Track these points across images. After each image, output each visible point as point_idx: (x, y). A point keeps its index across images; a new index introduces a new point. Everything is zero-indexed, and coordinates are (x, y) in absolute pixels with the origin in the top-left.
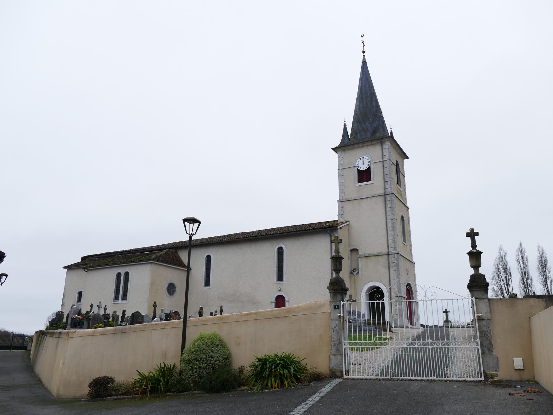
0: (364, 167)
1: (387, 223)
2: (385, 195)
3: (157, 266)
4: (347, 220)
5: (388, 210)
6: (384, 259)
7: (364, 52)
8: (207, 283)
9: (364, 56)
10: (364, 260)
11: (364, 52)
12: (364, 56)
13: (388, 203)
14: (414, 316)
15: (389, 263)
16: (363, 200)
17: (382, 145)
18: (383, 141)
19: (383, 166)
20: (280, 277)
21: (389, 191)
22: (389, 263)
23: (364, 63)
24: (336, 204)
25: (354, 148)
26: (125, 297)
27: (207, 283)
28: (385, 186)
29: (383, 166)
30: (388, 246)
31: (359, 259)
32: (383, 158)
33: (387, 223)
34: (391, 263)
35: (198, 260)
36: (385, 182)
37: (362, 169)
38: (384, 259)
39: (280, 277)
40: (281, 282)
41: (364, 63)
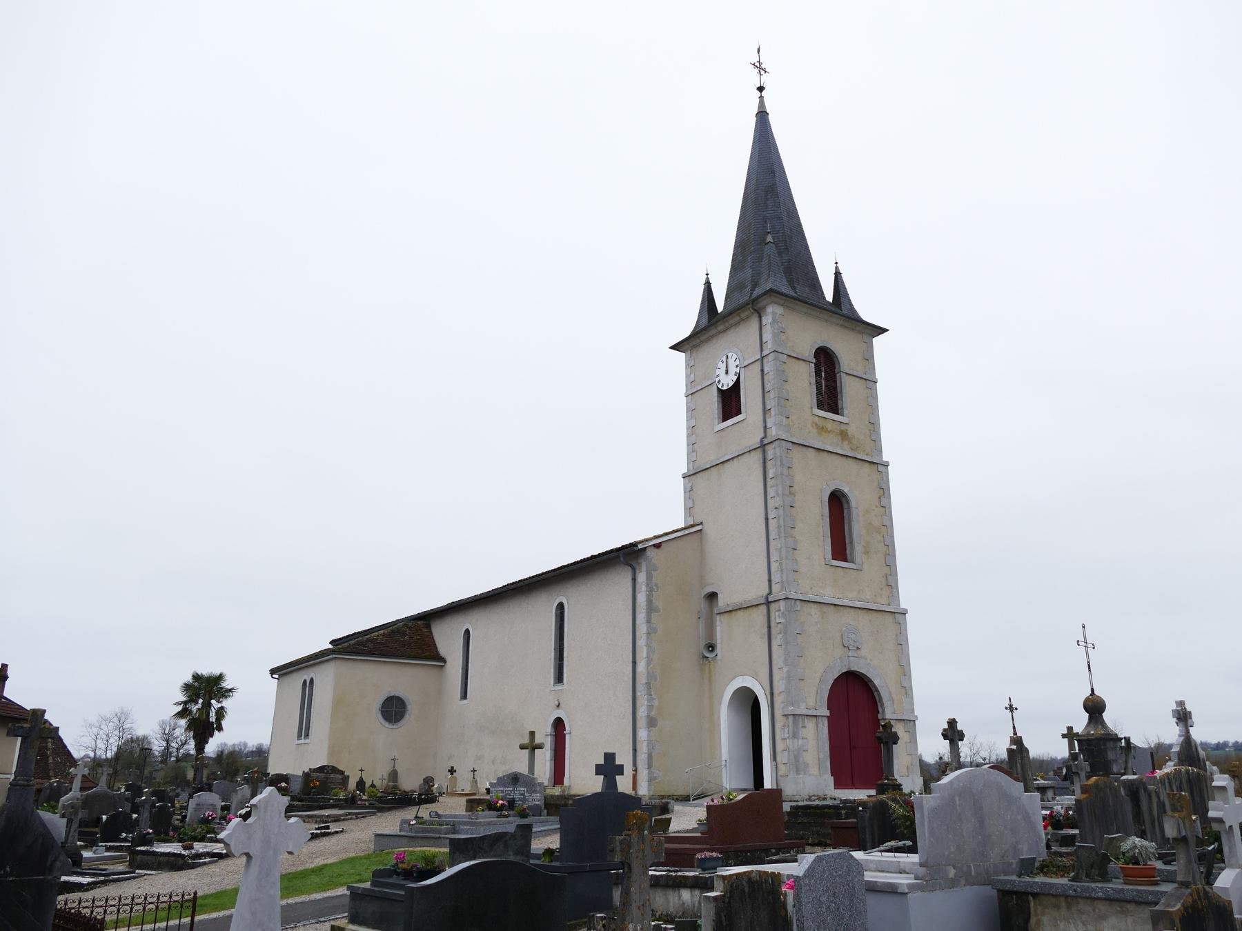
0: (727, 382)
1: (767, 519)
2: (763, 446)
3: (350, 664)
4: (698, 520)
5: (770, 483)
6: (759, 615)
7: (761, 89)
8: (464, 696)
9: (761, 97)
10: (725, 618)
11: (761, 89)
12: (761, 97)
13: (769, 464)
14: (419, 841)
15: (769, 627)
16: (726, 465)
17: (760, 317)
18: (760, 305)
19: (762, 371)
20: (559, 678)
21: (773, 433)
22: (769, 627)
23: (762, 115)
24: (679, 485)
25: (712, 337)
26: (307, 735)
27: (464, 696)
28: (765, 421)
29: (762, 371)
30: (770, 581)
31: (718, 617)
32: (762, 350)
33: (767, 519)
34: (773, 624)
35: (447, 638)
36: (765, 411)
37: (725, 388)
38: (759, 615)
39: (559, 678)
40: (559, 687)
41: (762, 115)
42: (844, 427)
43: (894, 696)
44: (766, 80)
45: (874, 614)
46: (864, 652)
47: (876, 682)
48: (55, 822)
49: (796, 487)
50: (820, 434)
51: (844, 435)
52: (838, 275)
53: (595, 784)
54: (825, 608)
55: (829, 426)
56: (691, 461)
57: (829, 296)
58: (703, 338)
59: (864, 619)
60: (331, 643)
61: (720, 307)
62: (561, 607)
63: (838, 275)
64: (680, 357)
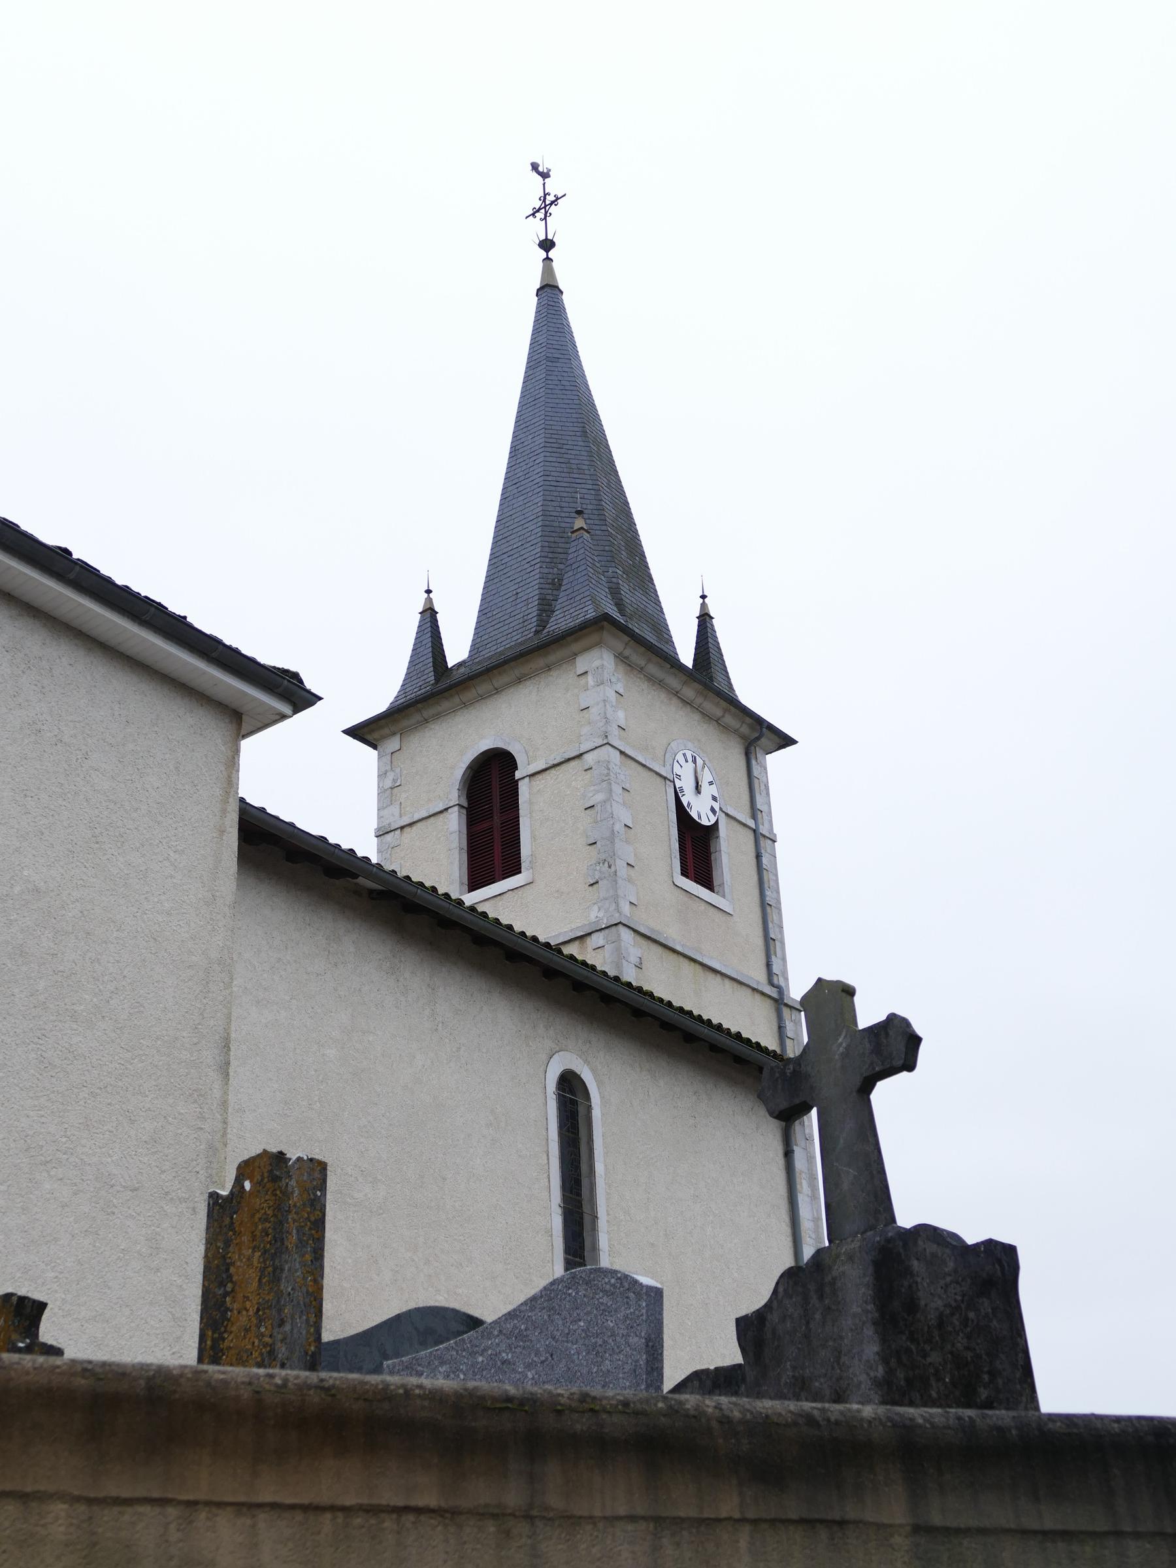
11: (547, 245)
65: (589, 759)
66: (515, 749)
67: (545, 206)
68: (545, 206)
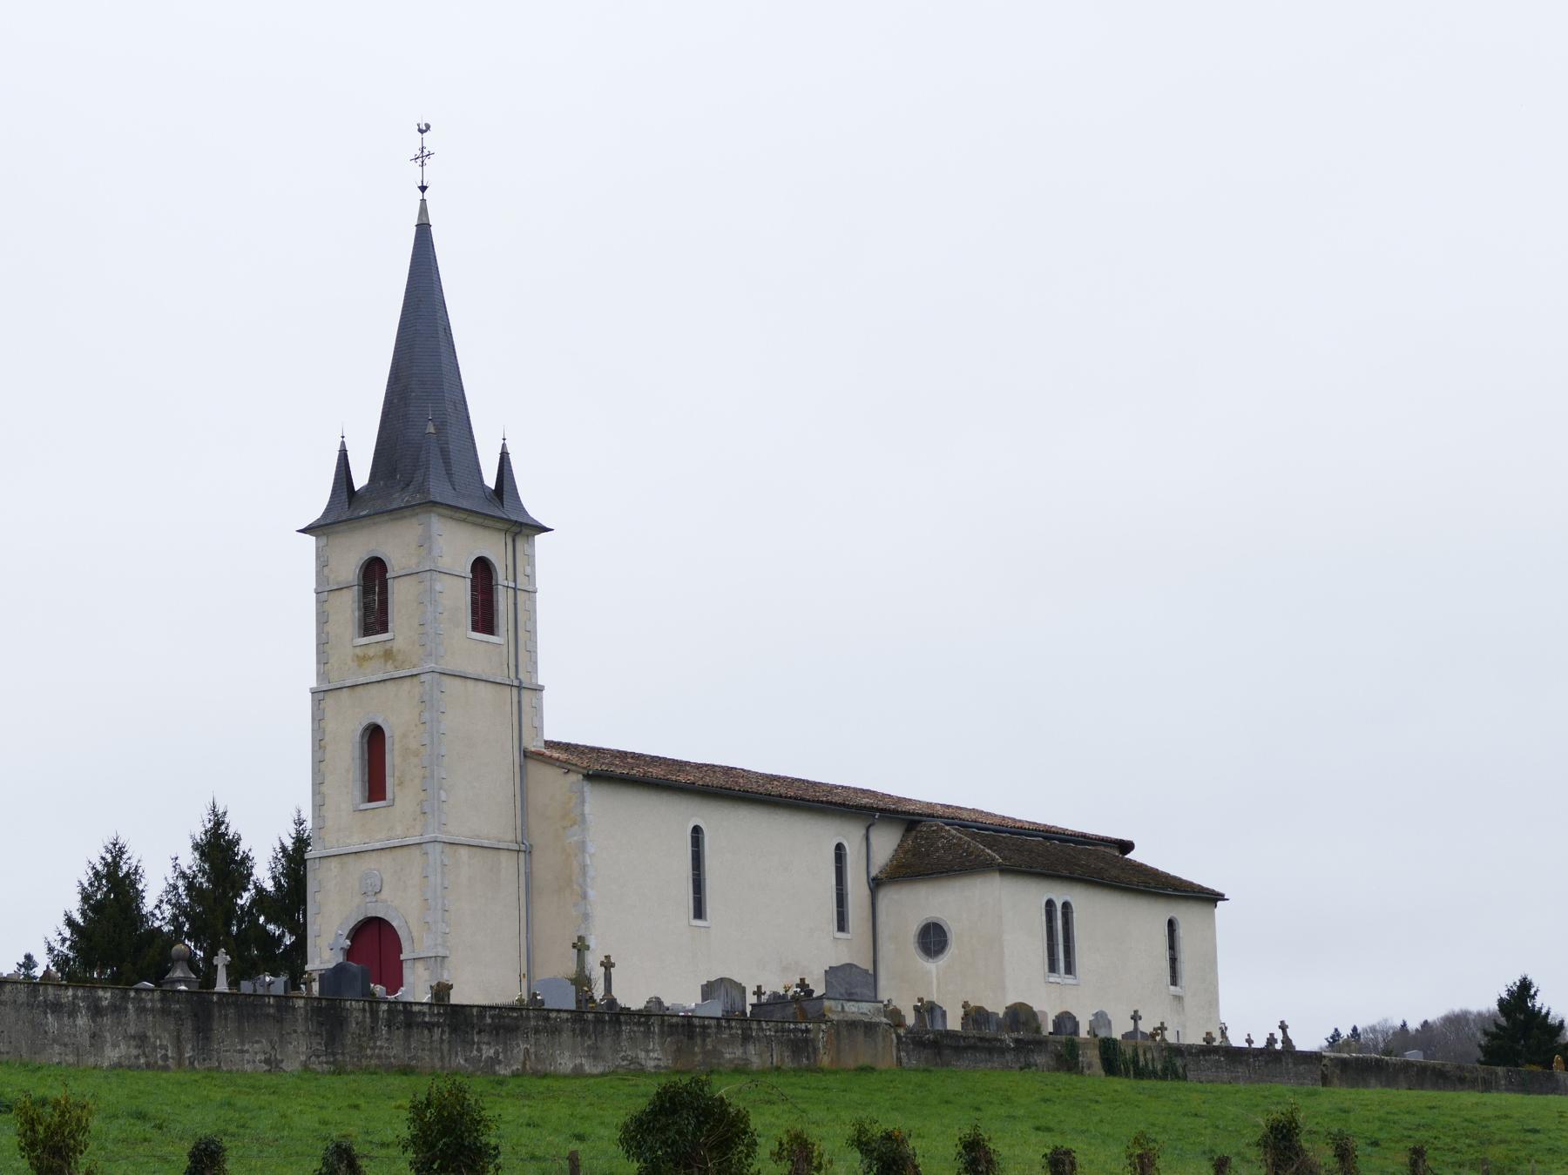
7: (423, 189)
9: (423, 201)
11: (423, 189)
12: (423, 201)
20: (699, 912)
26: (1069, 969)
39: (699, 912)
42: (388, 646)
43: (415, 934)
44: (414, 174)
45: (399, 851)
46: (384, 895)
47: (394, 924)
48: (1500, 1070)
49: (327, 738)
50: (360, 666)
51: (388, 655)
52: (504, 458)
53: (1130, 1027)
54: (345, 859)
55: (371, 652)
56: (321, 675)
57: (490, 480)
58: (457, 515)
59: (386, 858)
60: (246, 858)
61: (360, 478)
62: (697, 831)
63: (504, 458)
64: (310, 540)
65: (423, 678)
66: (379, 722)
67: (422, 157)
68: (422, 157)
